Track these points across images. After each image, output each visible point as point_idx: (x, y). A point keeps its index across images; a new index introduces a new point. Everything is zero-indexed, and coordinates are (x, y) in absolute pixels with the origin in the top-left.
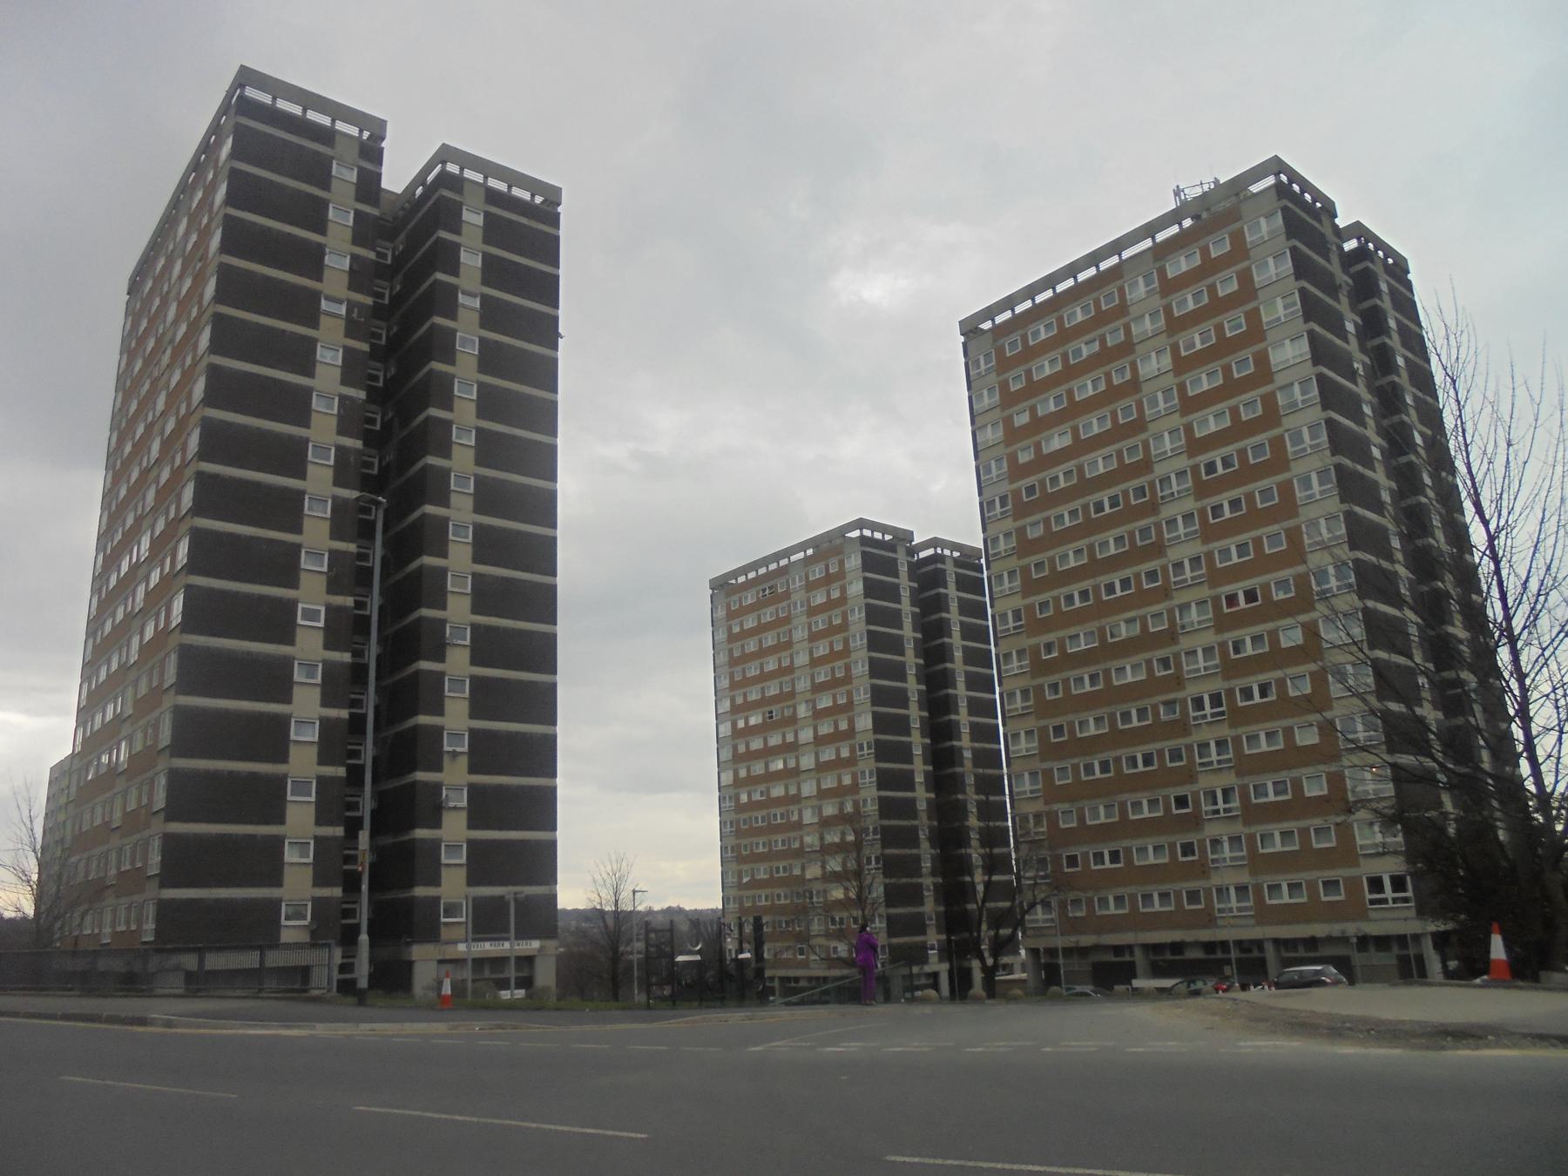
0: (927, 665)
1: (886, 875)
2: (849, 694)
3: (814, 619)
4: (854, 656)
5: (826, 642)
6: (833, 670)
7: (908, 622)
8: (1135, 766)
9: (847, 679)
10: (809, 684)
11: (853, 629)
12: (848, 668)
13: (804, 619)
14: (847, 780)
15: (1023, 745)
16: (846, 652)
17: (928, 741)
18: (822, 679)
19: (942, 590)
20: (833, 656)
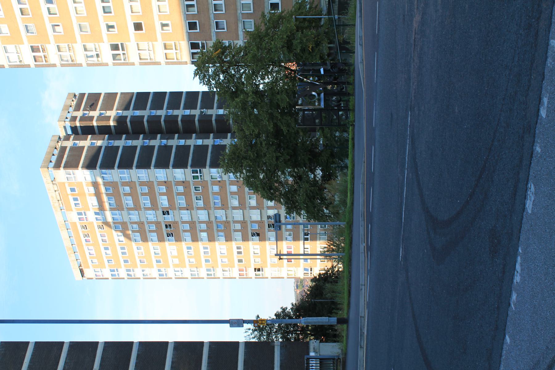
0: (144, 132)
1: (204, 166)
2: (160, 183)
3: (125, 206)
4: (134, 179)
5: (123, 198)
6: (143, 194)
7: (134, 143)
8: (192, 6)
9: (149, 184)
10: (185, 212)
11: (116, 179)
12: (142, 184)
13: (125, 213)
14: (216, 188)
15: (311, 79)
16: (131, 184)
17: (194, 135)
18: (218, 201)
19: (179, 119)
20: (133, 194)
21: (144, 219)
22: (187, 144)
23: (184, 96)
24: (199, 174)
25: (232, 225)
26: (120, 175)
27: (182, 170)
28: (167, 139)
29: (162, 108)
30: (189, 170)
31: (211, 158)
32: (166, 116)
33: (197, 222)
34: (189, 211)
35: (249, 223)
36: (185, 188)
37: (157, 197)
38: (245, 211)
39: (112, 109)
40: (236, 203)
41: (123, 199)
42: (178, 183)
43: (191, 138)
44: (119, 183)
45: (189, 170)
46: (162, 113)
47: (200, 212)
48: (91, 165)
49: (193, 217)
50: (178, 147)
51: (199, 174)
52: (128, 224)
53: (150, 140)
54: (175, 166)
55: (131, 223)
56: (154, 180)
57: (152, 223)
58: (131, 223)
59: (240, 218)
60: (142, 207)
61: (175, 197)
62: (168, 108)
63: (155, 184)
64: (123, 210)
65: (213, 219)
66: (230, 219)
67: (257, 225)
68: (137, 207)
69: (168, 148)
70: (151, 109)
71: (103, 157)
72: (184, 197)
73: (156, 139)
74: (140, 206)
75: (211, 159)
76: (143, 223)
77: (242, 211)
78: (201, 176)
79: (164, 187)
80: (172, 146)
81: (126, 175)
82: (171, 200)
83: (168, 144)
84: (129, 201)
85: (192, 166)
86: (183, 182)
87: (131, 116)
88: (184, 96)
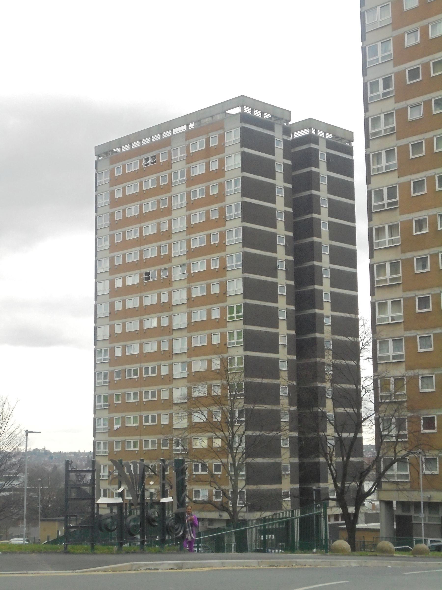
1: (246, 323)
4: (229, 225)
5: (203, 210)
10: (185, 249)
11: (229, 200)
13: (183, 188)
20: (208, 224)
21: (175, 238)
22: (280, 323)
23: (353, 316)
24: (235, 314)
25: (167, 314)
26: (234, 255)
27: (241, 292)
28: (286, 271)
29: (332, 262)
30: (242, 379)
31: (260, 332)
32: (322, 316)
33: (171, 313)
34: (185, 301)
35: (170, 386)
36: (216, 221)
37: (205, 307)
38: (186, 306)
39: (329, 169)
40: (197, 292)
41: (202, 209)
42: (223, 286)
43: (288, 303)
44: (224, 278)
45: (240, 301)
46: (328, 359)
47: (185, 317)
48: (252, 366)
49: (178, 308)
50: (276, 362)
51: (235, 314)
52: (169, 218)
53: (285, 246)
54: (246, 282)
55: (170, 221)
56: (226, 153)
57: (170, 249)
58: (170, 221)
59: (175, 301)
60: (191, 212)
61: (205, 282)
62: (332, 270)
63: (223, 254)
64: (188, 186)
65: (175, 334)
66: (175, 310)
67: (167, 422)
68: (191, 205)
69: (273, 272)
70: (331, 247)
71: (259, 181)
72: (205, 294)
73: (287, 254)
74: (192, 233)
75: (257, 331)
76: (169, 237)
77: (185, 326)
78: (233, 318)
79: (218, 267)
80: (276, 277)
81: (234, 213)
82: (200, 276)
83: (279, 271)
84: (198, 218)
85: (246, 305)
86: (225, 294)
87: (319, 197)
88: (353, 316)
